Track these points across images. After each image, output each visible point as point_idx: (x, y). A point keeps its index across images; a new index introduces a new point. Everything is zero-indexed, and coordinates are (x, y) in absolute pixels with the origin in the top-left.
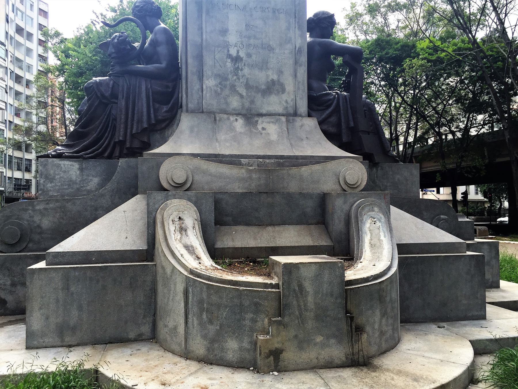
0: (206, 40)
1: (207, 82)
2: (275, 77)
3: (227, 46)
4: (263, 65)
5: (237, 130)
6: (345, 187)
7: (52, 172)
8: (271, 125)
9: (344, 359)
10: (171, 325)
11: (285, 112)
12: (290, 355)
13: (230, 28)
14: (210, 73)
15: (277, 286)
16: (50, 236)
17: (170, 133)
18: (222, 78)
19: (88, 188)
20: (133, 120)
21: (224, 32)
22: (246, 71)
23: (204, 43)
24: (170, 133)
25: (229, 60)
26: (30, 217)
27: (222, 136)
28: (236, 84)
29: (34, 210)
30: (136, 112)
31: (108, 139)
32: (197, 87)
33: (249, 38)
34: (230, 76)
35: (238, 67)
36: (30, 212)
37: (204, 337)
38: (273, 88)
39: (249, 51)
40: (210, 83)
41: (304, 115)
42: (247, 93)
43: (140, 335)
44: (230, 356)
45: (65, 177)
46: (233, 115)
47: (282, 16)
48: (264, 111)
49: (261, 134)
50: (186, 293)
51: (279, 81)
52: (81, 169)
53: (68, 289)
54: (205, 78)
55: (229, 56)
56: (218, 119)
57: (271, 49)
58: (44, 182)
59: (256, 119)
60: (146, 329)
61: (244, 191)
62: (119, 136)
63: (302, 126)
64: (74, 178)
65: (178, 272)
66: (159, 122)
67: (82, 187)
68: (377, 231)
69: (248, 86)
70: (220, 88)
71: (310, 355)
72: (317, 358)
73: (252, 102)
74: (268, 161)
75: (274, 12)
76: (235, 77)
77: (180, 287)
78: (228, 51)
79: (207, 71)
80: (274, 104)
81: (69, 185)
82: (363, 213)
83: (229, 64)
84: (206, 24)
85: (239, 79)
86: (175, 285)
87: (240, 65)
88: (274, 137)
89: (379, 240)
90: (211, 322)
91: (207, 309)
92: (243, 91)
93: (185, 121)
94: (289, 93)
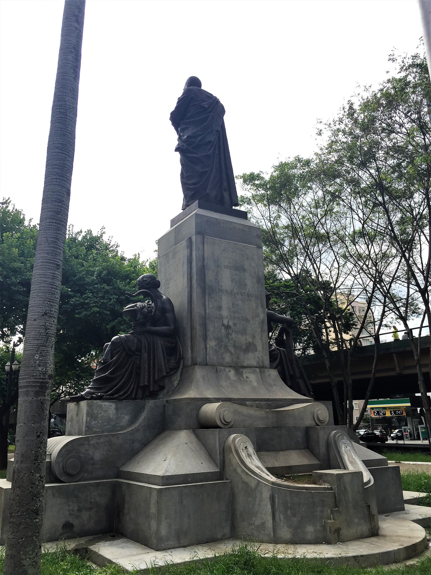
0: (209, 313)
1: (210, 343)
2: (251, 340)
3: (221, 318)
4: (243, 332)
5: (232, 378)
6: (317, 422)
7: (96, 412)
8: (251, 374)
9: (368, 532)
10: (258, 522)
11: (258, 365)
12: (344, 532)
13: (223, 306)
14: (211, 336)
15: (331, 489)
16: (99, 466)
17: (175, 378)
18: (219, 340)
19: (121, 424)
20: (154, 368)
21: (220, 308)
22: (234, 335)
23: (207, 316)
24: (175, 378)
25: (223, 328)
26: (86, 450)
27: (224, 383)
28: (228, 344)
29: (89, 445)
30: (156, 363)
31: (133, 384)
32: (203, 346)
33: (235, 312)
34: (224, 339)
35: (229, 333)
36: (86, 446)
37: (290, 526)
38: (250, 348)
39: (235, 322)
40: (212, 344)
41: (267, 367)
42: (234, 351)
43: (224, 535)
44: (309, 537)
45: (105, 415)
46: (227, 367)
47: (253, 298)
48: (245, 364)
49: (247, 381)
50: (272, 499)
51: (253, 342)
52: (117, 409)
53: (182, 502)
54: (208, 340)
55: (223, 325)
56: (218, 370)
57: (247, 320)
58: (90, 420)
59: (242, 370)
60: (227, 530)
61: (265, 426)
62: (144, 381)
63: (269, 375)
64: (111, 416)
65: (263, 485)
66: (171, 370)
67: (117, 423)
68: (349, 452)
69: (235, 346)
70: (219, 347)
71: (353, 531)
72: (356, 533)
73: (238, 358)
74: (261, 403)
75: (248, 296)
76: (227, 340)
77: (266, 494)
78: (223, 321)
79: (210, 334)
80: (251, 359)
81: (108, 422)
82: (339, 441)
83: (223, 331)
84: (209, 302)
85: (229, 341)
86: (261, 493)
87: (230, 331)
88: (255, 384)
89: (354, 459)
90: (294, 515)
91: (291, 507)
92: (232, 350)
93: (199, 373)
94: (259, 351)
